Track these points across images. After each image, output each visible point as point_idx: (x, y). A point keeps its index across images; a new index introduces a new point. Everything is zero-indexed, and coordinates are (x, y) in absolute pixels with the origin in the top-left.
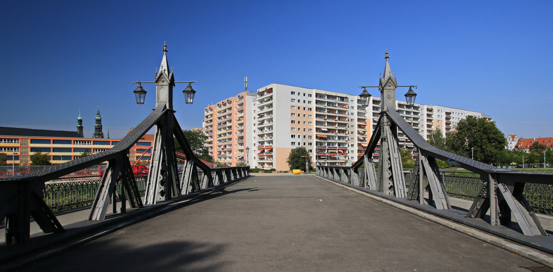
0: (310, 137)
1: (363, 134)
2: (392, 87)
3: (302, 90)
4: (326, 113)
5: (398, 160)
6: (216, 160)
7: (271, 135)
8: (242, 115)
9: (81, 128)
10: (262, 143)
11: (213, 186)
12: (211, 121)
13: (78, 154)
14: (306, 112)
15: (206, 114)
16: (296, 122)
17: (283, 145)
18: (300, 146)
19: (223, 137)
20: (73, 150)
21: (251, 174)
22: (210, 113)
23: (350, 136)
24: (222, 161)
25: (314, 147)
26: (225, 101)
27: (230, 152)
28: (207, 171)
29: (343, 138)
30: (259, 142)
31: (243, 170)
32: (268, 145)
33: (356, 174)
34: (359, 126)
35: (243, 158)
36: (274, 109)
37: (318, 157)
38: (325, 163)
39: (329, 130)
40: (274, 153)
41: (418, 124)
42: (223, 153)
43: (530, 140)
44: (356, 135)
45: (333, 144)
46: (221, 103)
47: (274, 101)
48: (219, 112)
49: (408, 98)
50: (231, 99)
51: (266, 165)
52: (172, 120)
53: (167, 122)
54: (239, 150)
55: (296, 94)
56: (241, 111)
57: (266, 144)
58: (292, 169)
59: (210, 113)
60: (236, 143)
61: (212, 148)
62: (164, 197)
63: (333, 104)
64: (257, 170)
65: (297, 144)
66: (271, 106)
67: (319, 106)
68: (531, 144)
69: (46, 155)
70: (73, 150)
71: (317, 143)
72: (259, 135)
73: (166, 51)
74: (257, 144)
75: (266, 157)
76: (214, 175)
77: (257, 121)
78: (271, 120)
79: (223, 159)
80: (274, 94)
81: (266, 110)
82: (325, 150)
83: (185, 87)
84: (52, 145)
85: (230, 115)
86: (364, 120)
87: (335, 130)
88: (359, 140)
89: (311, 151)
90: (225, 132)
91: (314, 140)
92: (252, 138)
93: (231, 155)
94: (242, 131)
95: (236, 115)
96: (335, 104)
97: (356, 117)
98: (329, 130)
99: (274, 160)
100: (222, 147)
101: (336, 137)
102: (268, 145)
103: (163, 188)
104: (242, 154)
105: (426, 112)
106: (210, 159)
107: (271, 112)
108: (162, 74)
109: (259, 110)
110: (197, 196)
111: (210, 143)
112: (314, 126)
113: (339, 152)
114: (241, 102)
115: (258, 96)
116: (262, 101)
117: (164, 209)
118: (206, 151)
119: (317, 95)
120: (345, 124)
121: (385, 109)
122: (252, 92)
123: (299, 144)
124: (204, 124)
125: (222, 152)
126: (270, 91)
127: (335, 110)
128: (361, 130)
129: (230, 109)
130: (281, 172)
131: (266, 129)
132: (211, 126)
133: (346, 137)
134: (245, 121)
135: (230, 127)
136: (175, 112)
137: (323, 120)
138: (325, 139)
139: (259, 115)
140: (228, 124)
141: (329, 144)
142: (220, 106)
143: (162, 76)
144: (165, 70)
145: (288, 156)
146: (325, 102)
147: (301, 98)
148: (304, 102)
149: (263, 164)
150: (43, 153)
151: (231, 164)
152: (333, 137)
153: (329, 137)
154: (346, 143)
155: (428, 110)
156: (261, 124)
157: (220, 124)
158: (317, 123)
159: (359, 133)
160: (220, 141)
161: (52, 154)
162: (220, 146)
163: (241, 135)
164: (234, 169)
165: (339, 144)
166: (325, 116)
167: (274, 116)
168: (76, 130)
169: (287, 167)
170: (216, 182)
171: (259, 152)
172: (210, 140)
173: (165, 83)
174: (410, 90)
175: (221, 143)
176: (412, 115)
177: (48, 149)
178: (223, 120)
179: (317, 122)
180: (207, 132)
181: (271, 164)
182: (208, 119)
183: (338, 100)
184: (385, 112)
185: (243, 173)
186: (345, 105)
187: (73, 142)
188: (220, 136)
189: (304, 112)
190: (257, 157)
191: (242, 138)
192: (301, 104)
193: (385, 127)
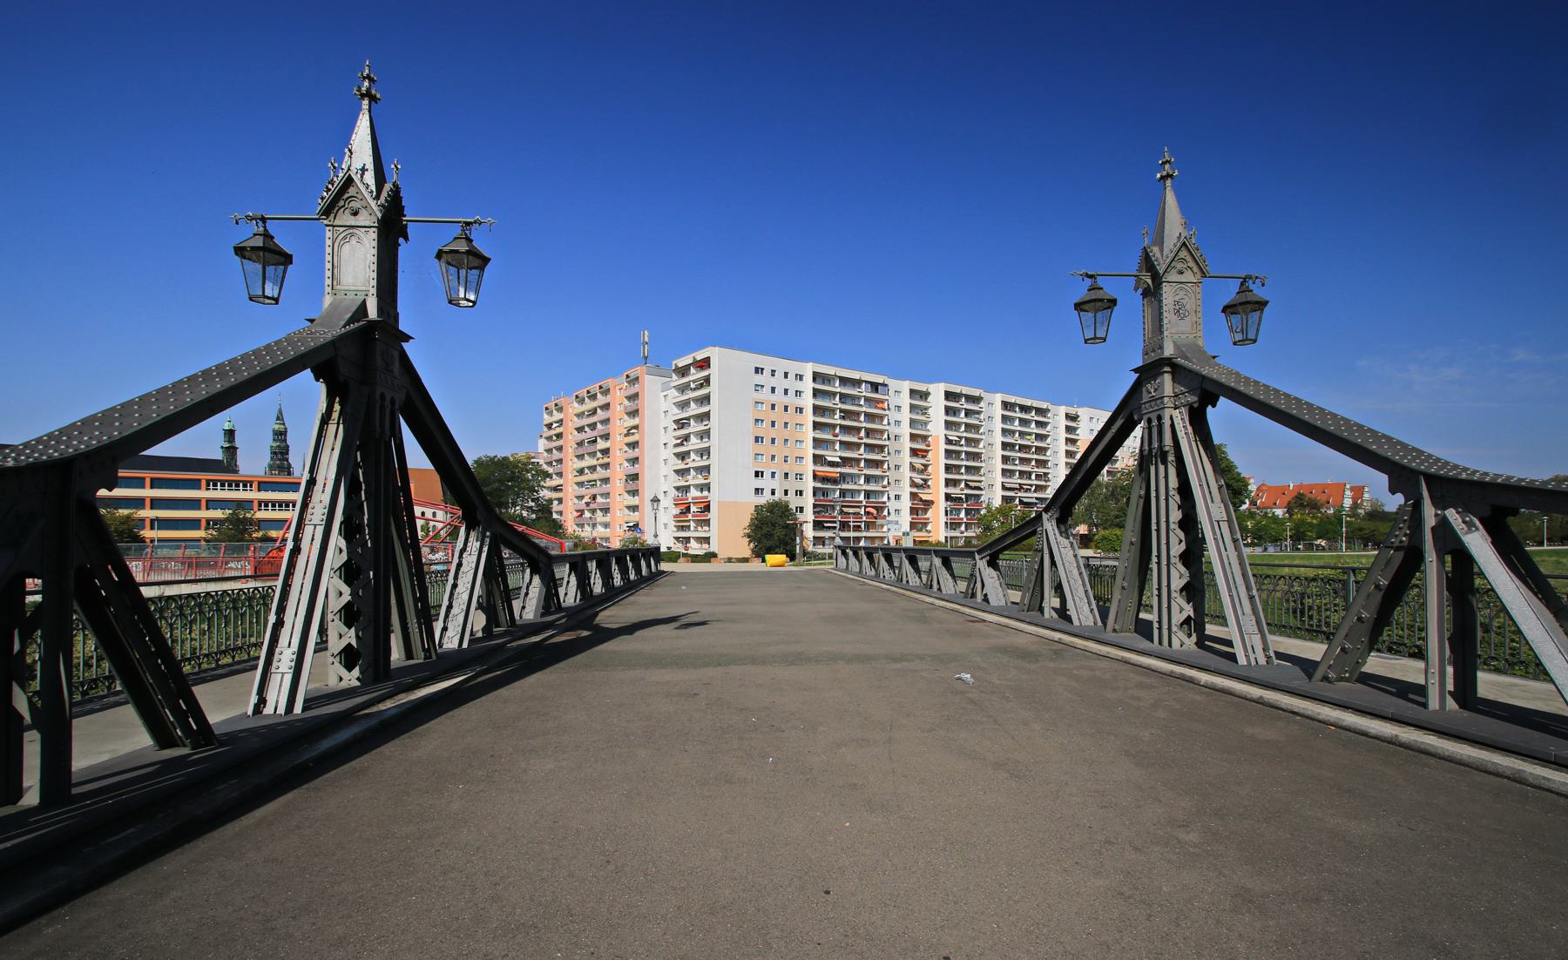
0: (799, 476)
1: (922, 472)
2: (1188, 276)
3: (782, 365)
4: (837, 420)
5: (1225, 526)
6: (570, 530)
7: (706, 470)
8: (636, 421)
9: (231, 451)
10: (686, 489)
11: (559, 608)
12: (559, 436)
13: (218, 514)
14: (791, 416)
15: (547, 419)
16: (767, 441)
17: (735, 496)
18: (777, 497)
19: (588, 476)
20: (204, 504)
21: (664, 566)
22: (557, 416)
23: (892, 474)
24: (587, 533)
25: (808, 501)
26: (595, 388)
27: (606, 510)
28: (541, 563)
29: (877, 479)
30: (678, 489)
31: (639, 561)
32: (699, 494)
33: (990, 571)
34: (914, 452)
35: (636, 526)
36: (714, 407)
37: (818, 525)
38: (858, 539)
39: (846, 461)
40: (713, 515)
41: (1045, 449)
42: (587, 514)
43: (1282, 491)
44: (906, 473)
45: (853, 492)
46: (583, 393)
47: (714, 389)
48: (580, 415)
49: (1235, 319)
50: (609, 383)
51: (693, 544)
52: (396, 367)
53: (368, 373)
54: (629, 508)
55: (767, 372)
56: (634, 413)
57: (694, 493)
58: (760, 553)
59: (557, 416)
60: (621, 491)
61: (560, 501)
62: (356, 672)
63: (853, 399)
64: (673, 557)
65: (767, 493)
66: (706, 399)
67: (820, 403)
68: (1287, 498)
69: (128, 517)
70: (204, 504)
71: (815, 491)
72: (677, 472)
73: (368, 95)
74: (674, 493)
75: (692, 524)
76: (562, 571)
77: (671, 437)
78: (705, 434)
79: (587, 528)
80: (714, 371)
81: (694, 409)
82: (833, 507)
83: (446, 238)
84: (147, 493)
85: (606, 421)
86: (925, 438)
87: (858, 461)
88: (913, 484)
89: (802, 510)
90: (593, 462)
91: (809, 484)
92: (660, 476)
93: (607, 519)
94: (634, 461)
95: (621, 423)
96: (859, 398)
97: (905, 430)
98: (846, 461)
99: (713, 532)
100: (586, 499)
101: (859, 476)
102: (699, 494)
103: (351, 637)
104: (635, 517)
105: (1063, 422)
106: (556, 528)
107: (707, 416)
108: (349, 181)
109: (676, 410)
110: (505, 657)
111: (556, 489)
112: (809, 451)
113: (868, 513)
114: (633, 390)
115: (674, 377)
116: (683, 389)
117: (327, 744)
118: (545, 509)
119: (816, 377)
120: (881, 448)
121: (1169, 351)
122: (659, 370)
123: (773, 493)
124: (542, 445)
125: (590, 514)
126: (704, 364)
127: (858, 414)
128: (918, 462)
129: (606, 407)
130: (729, 560)
131: (693, 456)
132: (560, 449)
133: (883, 477)
134: (642, 436)
135: (606, 452)
136: (407, 338)
137: (830, 437)
138: (835, 481)
139: (676, 422)
140: (601, 444)
141: (843, 493)
142: (582, 401)
143: (352, 191)
144: (364, 170)
145: (747, 522)
146: (834, 394)
147: (780, 383)
148: (786, 392)
149: (687, 540)
150: (124, 512)
151: (607, 539)
152: (853, 478)
153: (843, 477)
154: (883, 493)
155: (1068, 416)
156: (681, 444)
157: (580, 444)
158: (817, 443)
159: (913, 468)
160: (580, 484)
161: (147, 513)
162: (581, 498)
163: (632, 470)
164: (620, 556)
165: (868, 494)
166: (833, 426)
167: (714, 423)
168: (218, 455)
169: (745, 549)
170: (569, 594)
171: (677, 511)
172: (556, 481)
173: (364, 219)
174: (1244, 288)
175: (583, 491)
176: (1033, 428)
177: (138, 503)
178: (589, 434)
179: (815, 440)
180: (550, 464)
181: (707, 540)
182: (553, 432)
183: (864, 391)
184: (1169, 362)
185: (643, 563)
186: (882, 401)
187: (204, 483)
188: (581, 471)
189: (786, 417)
190: (672, 525)
191: (634, 477)
192: (779, 398)
193: (1167, 414)
